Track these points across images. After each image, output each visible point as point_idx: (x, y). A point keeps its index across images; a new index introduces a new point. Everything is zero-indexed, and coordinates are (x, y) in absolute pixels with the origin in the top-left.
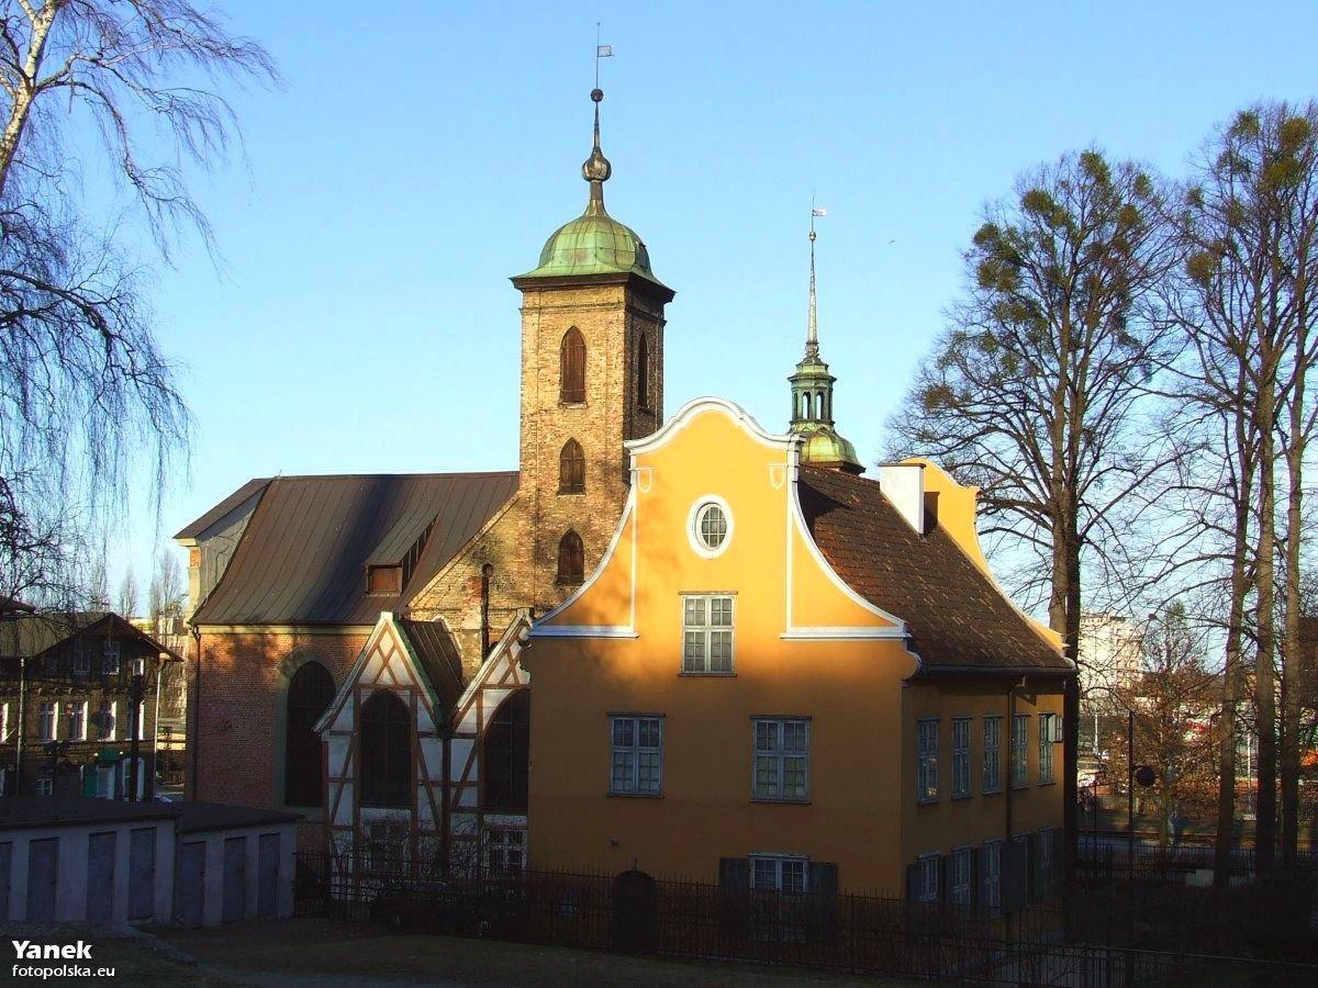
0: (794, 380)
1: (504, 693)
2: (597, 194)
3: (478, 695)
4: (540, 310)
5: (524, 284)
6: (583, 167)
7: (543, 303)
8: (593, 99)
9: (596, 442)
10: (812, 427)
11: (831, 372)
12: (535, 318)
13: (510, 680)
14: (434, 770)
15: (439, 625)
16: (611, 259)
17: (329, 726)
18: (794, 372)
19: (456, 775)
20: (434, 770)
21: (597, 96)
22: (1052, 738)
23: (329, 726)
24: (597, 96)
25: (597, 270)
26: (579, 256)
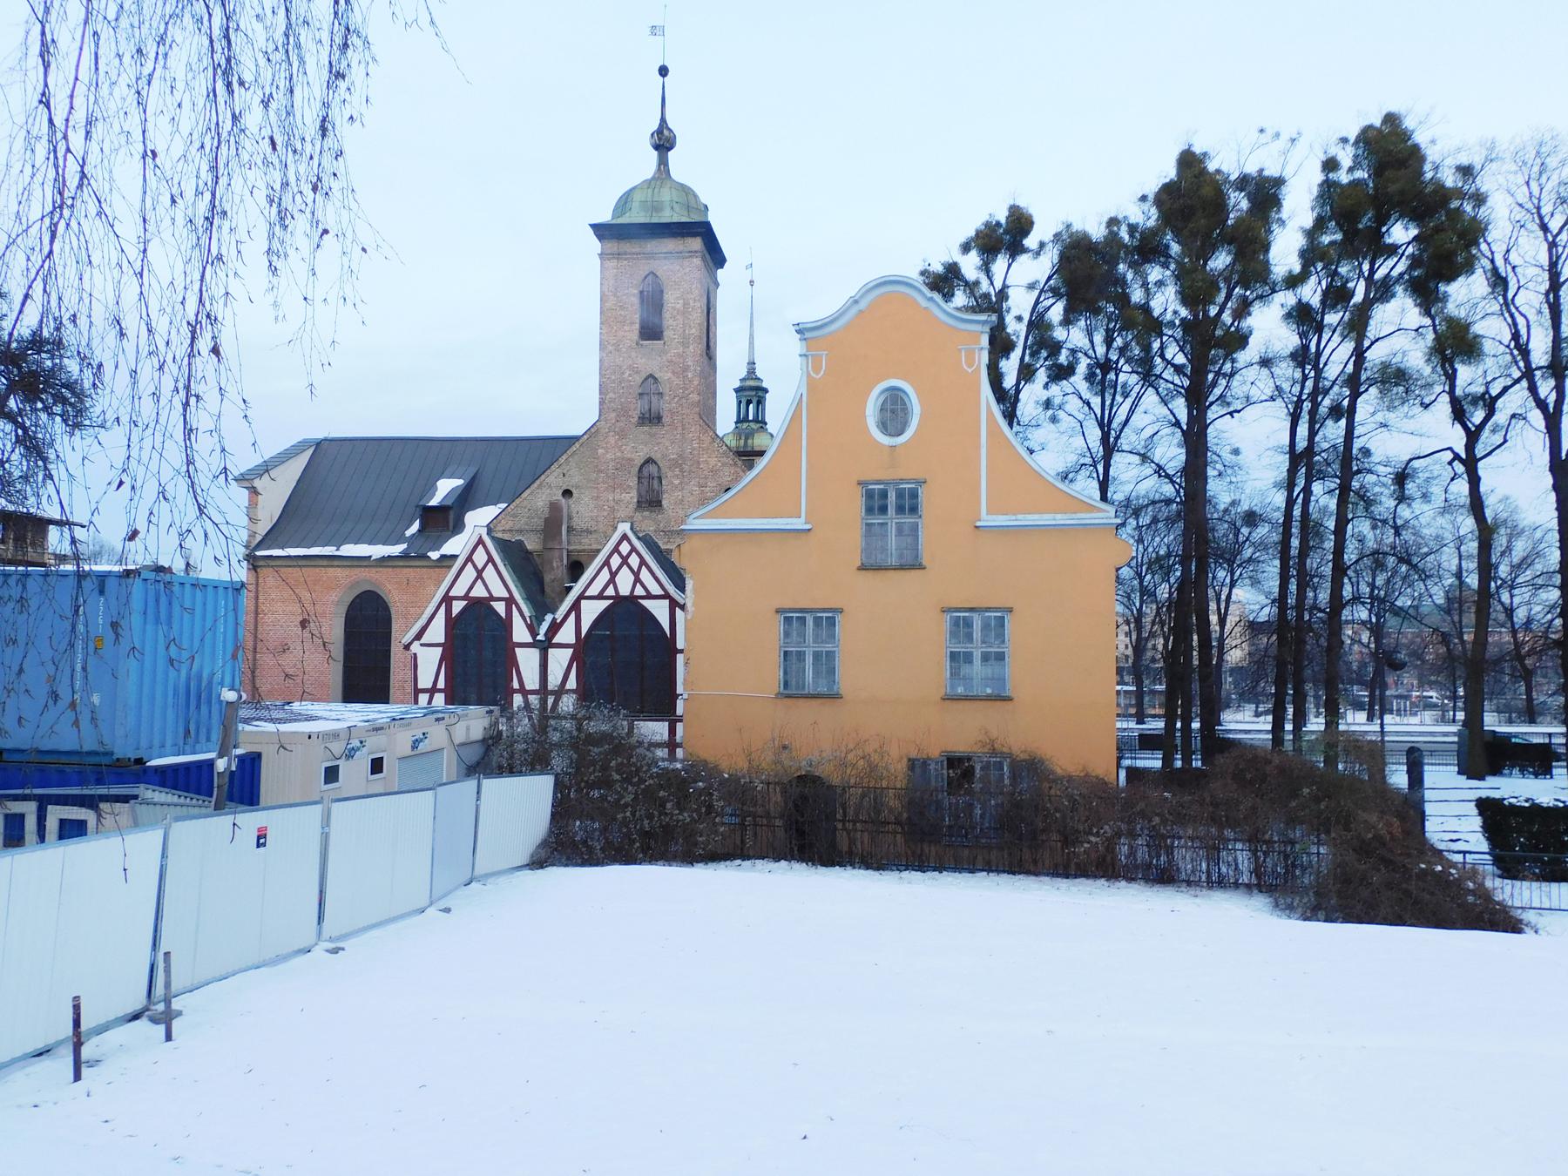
0: (737, 390)
1: (605, 604)
2: (663, 163)
3: (576, 607)
4: (618, 256)
5: (601, 231)
6: (652, 135)
7: (621, 250)
8: (661, 74)
9: (674, 378)
10: (753, 425)
11: (764, 385)
12: (613, 263)
13: (610, 591)
14: (532, 681)
15: (520, 543)
16: (686, 213)
17: (419, 636)
18: (737, 384)
19: (554, 680)
20: (532, 681)
21: (663, 71)
22: (425, 681)
23: (419, 636)
24: (663, 71)
25: (676, 219)
26: (656, 207)
